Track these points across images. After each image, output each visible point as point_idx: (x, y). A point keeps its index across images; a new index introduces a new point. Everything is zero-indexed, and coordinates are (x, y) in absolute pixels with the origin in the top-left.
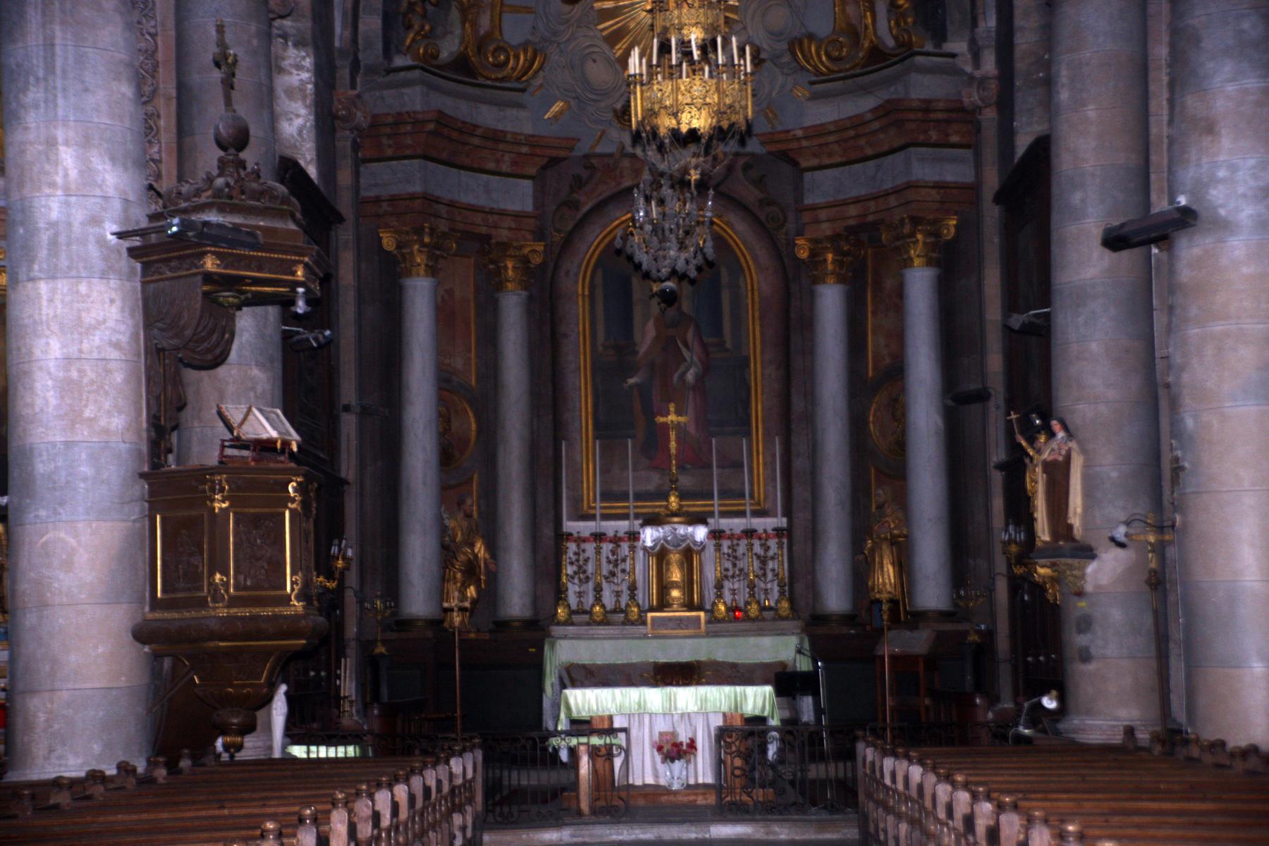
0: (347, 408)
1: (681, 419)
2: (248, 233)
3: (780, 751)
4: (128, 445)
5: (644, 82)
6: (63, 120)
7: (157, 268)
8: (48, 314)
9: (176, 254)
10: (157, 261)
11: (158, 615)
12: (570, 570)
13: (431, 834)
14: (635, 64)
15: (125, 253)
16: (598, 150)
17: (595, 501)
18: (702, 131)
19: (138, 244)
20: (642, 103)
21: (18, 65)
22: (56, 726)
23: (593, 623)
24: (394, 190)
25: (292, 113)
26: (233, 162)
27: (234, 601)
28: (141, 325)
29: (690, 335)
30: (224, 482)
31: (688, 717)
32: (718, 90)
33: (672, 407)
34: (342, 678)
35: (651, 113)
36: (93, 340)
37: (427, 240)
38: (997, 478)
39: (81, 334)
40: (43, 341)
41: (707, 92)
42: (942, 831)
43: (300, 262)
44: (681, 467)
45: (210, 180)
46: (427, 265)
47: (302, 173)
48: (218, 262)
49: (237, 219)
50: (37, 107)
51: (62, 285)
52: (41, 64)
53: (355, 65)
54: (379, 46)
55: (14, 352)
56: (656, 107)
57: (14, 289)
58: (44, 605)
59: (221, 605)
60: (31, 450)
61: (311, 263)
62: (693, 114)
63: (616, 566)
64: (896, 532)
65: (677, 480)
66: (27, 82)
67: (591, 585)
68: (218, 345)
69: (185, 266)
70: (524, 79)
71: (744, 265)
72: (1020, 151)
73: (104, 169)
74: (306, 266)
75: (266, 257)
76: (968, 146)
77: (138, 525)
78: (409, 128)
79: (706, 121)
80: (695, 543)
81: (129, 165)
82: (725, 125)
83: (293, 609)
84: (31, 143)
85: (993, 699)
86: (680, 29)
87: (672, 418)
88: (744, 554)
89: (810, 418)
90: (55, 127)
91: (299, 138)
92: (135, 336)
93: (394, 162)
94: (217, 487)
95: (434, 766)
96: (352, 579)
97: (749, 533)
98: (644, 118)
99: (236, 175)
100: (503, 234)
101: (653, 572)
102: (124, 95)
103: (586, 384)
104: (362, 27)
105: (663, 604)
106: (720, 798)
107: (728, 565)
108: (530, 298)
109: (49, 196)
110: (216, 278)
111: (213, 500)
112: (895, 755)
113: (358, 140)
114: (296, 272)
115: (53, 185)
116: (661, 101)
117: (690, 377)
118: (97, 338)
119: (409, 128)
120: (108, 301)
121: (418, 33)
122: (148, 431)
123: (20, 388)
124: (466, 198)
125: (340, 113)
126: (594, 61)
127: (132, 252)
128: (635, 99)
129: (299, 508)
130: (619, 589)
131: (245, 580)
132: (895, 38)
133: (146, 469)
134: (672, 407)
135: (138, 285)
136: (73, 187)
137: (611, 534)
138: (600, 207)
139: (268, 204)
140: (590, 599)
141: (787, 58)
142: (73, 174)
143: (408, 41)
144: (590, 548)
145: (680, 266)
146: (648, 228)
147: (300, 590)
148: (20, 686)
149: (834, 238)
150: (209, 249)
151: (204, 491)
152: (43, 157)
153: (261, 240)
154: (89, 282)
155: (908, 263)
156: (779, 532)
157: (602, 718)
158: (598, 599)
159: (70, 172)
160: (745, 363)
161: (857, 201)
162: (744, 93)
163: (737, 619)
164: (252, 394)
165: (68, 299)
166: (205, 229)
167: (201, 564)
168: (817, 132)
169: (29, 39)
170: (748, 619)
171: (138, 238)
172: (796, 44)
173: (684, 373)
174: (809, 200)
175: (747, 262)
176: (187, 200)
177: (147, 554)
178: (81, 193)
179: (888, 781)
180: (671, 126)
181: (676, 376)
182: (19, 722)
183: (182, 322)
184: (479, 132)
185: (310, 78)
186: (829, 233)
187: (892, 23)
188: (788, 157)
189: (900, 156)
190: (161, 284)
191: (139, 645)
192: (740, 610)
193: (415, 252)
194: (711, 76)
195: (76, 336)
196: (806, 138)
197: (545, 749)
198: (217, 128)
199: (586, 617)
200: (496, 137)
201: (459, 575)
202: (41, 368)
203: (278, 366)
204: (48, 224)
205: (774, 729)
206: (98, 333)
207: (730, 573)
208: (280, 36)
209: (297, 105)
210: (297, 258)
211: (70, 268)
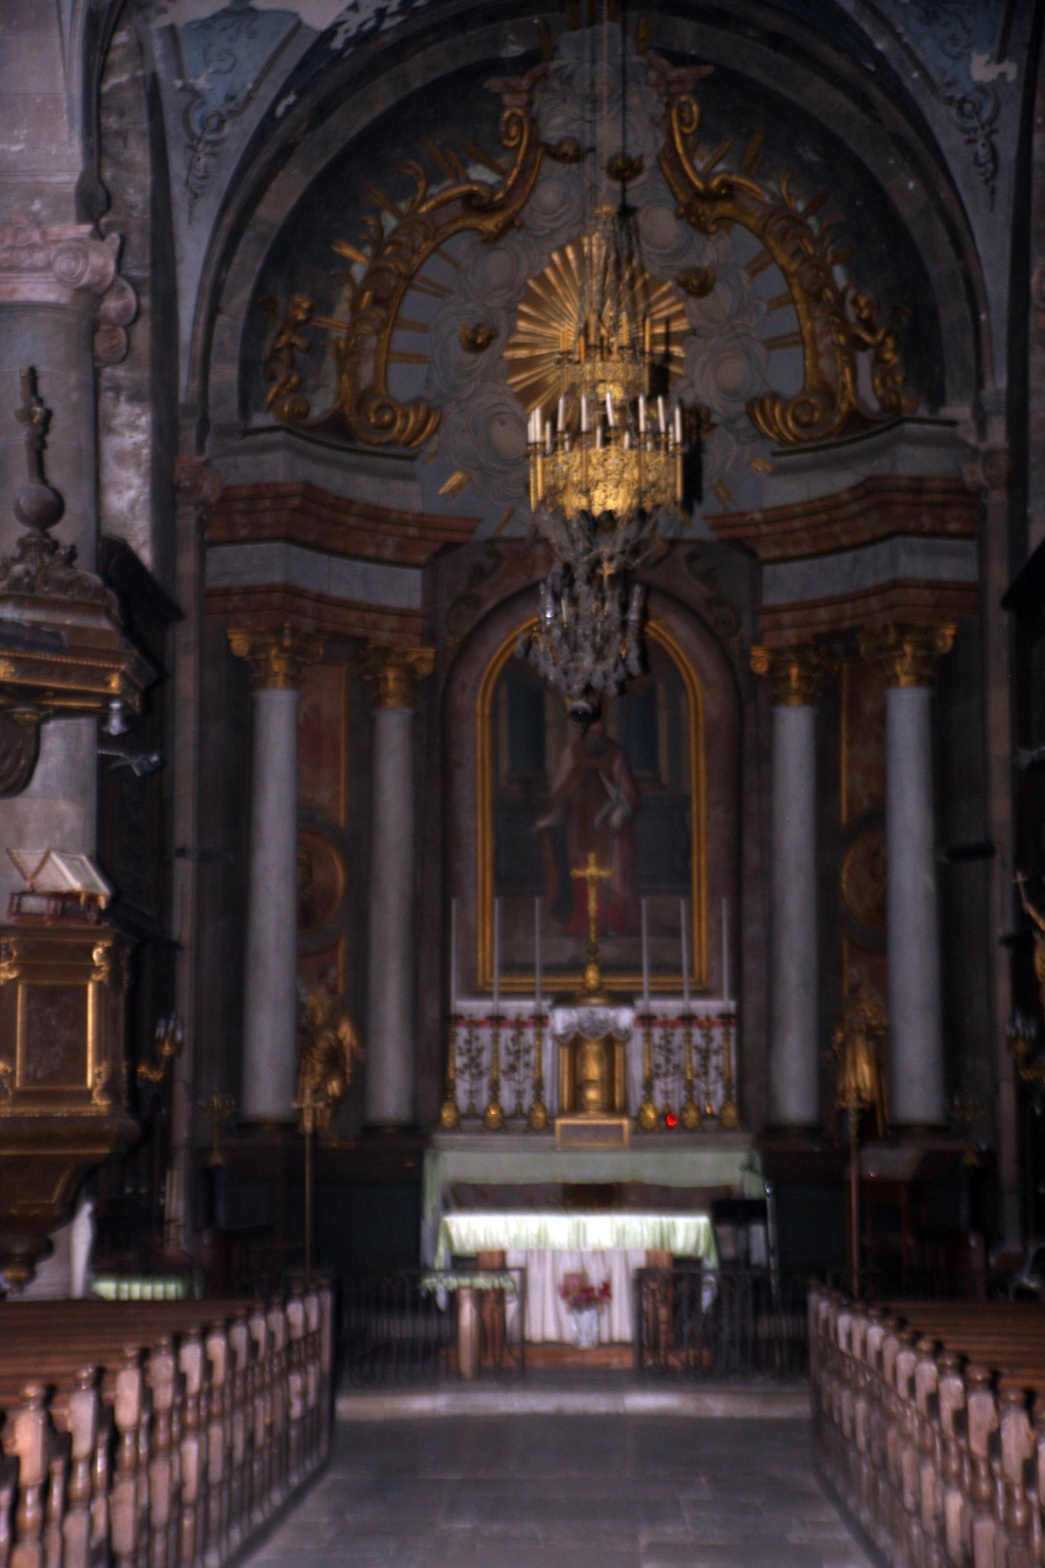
0: (182, 852)
1: (604, 873)
2: (50, 634)
3: (717, 1301)
5: (547, 452)
12: (459, 1061)
13: (259, 1403)
14: (535, 429)
16: (506, 533)
17: (492, 975)
18: (619, 514)
20: (543, 479)
23: (486, 1128)
24: (250, 579)
27: (21, 1097)
29: (617, 766)
30: (11, 946)
31: (601, 1254)
32: (638, 463)
33: (592, 857)
35: (553, 492)
37: (287, 642)
38: (1003, 956)
41: (624, 466)
42: (904, 1414)
44: (602, 933)
46: (286, 675)
47: (130, 558)
53: (204, 424)
54: (234, 403)
56: (561, 484)
62: (608, 493)
63: (518, 1058)
64: (874, 1022)
65: (597, 950)
67: (485, 1082)
70: (415, 444)
71: (687, 681)
72: (1034, 544)
74: (123, 675)
75: (72, 664)
76: (969, 536)
79: (624, 501)
80: (618, 1030)
82: (648, 505)
85: (992, 1239)
86: (594, 387)
87: (591, 871)
88: (680, 1047)
89: (766, 874)
95: (267, 1310)
96: (184, 1068)
97: (688, 1019)
98: (545, 498)
100: (383, 637)
101: (565, 1068)
103: (484, 825)
104: (213, 378)
105: (577, 1105)
106: (640, 1359)
107: (660, 1059)
108: (416, 719)
112: (853, 1312)
116: (566, 476)
117: (616, 818)
119: (268, 503)
121: (283, 385)
124: (339, 591)
126: (503, 423)
128: (536, 473)
130: (521, 1088)
132: (881, 400)
134: (592, 857)
137: (511, 1016)
138: (507, 604)
139: (77, 598)
140: (484, 1097)
141: (744, 423)
143: (270, 396)
144: (485, 1034)
145: (597, 680)
146: (557, 633)
149: (800, 649)
153: (66, 641)
155: (892, 681)
156: (725, 1018)
157: (491, 1254)
158: (495, 1099)
160: (684, 803)
161: (830, 602)
162: (672, 468)
163: (670, 1129)
168: (781, 515)
170: (683, 1127)
172: (755, 405)
173: (607, 817)
174: (769, 599)
175: (690, 677)
179: (843, 1344)
180: (581, 508)
181: (598, 819)
184: (355, 509)
185: (146, 441)
186: (794, 641)
187: (877, 382)
188: (743, 546)
189: (884, 548)
192: (673, 1117)
194: (631, 447)
196: (767, 522)
197: (416, 1293)
199: (479, 1123)
200: (376, 516)
201: (318, 1067)
203: (92, 799)
205: (711, 1272)
207: (662, 1071)
208: (109, 389)
210: (111, 666)
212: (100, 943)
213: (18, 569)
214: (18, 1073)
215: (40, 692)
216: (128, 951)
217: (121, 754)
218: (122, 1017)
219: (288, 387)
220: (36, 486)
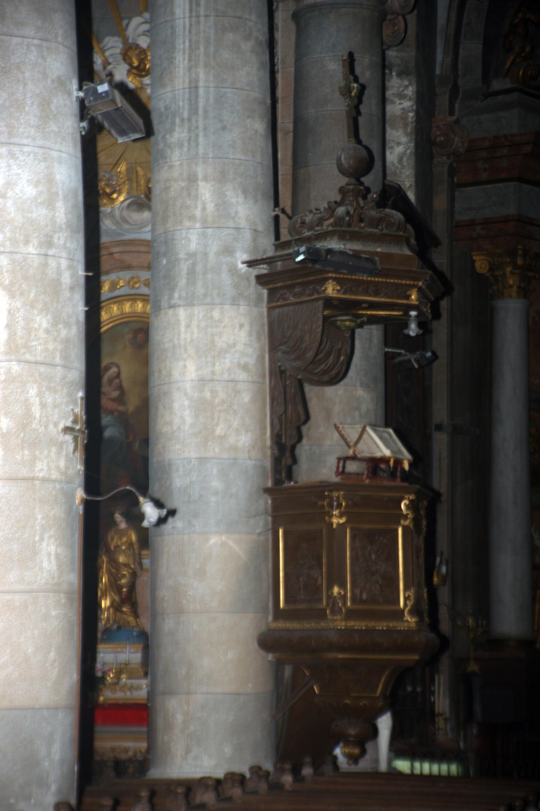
0: (439, 428)
4: (253, 462)
6: (203, 158)
7: (282, 295)
8: (186, 339)
9: (299, 280)
10: (282, 288)
11: (281, 624)
15: (253, 281)
19: (265, 271)
21: (166, 108)
22: (192, 728)
25: (394, 141)
26: (353, 192)
27: (351, 614)
28: (267, 348)
30: (341, 498)
34: (436, 695)
36: (224, 363)
37: (520, 261)
39: (214, 357)
40: (181, 364)
43: (414, 286)
45: (331, 209)
46: (519, 287)
48: (338, 288)
49: (356, 246)
50: (181, 146)
51: (199, 311)
52: (186, 107)
55: (156, 375)
57: (157, 316)
58: (180, 611)
59: (339, 617)
60: (170, 465)
61: (424, 287)
66: (173, 123)
68: (334, 366)
69: (307, 291)
73: (237, 202)
74: (420, 290)
75: (382, 282)
77: (262, 538)
78: (505, 151)
81: (259, 197)
83: (406, 625)
84: (176, 180)
90: (196, 165)
91: (399, 166)
92: (261, 358)
93: (489, 186)
94: (335, 504)
99: (355, 204)
102: (256, 131)
109: (189, 228)
110: (335, 302)
111: (331, 516)
113: (455, 165)
114: (410, 296)
115: (192, 218)
118: (227, 361)
119: (505, 151)
120: (238, 326)
122: (272, 448)
123: (161, 407)
125: (438, 139)
127: (261, 280)
129: (411, 526)
131: (361, 594)
133: (269, 484)
135: (265, 310)
136: (210, 219)
139: (385, 231)
142: (210, 207)
147: (413, 606)
148: (160, 687)
150: (330, 275)
151: (323, 507)
152: (185, 193)
154: (222, 309)
159: (208, 206)
164: (357, 414)
165: (203, 324)
166: (329, 257)
167: (320, 578)
169: (177, 83)
171: (265, 266)
176: (311, 228)
177: (270, 565)
178: (216, 225)
182: (160, 722)
183: (304, 345)
185: (412, 106)
190: (285, 309)
191: (263, 653)
193: (508, 275)
195: (209, 359)
198: (339, 159)
202: (179, 389)
203: (381, 386)
204: (188, 254)
206: (228, 355)
209: (399, 133)
210: (412, 283)
211: (205, 295)
212: (407, 497)
213: (341, 210)
214: (349, 595)
215: (358, 304)
216: (425, 503)
217: (403, 351)
218: (422, 553)
219: (523, 55)
220: (353, 144)
